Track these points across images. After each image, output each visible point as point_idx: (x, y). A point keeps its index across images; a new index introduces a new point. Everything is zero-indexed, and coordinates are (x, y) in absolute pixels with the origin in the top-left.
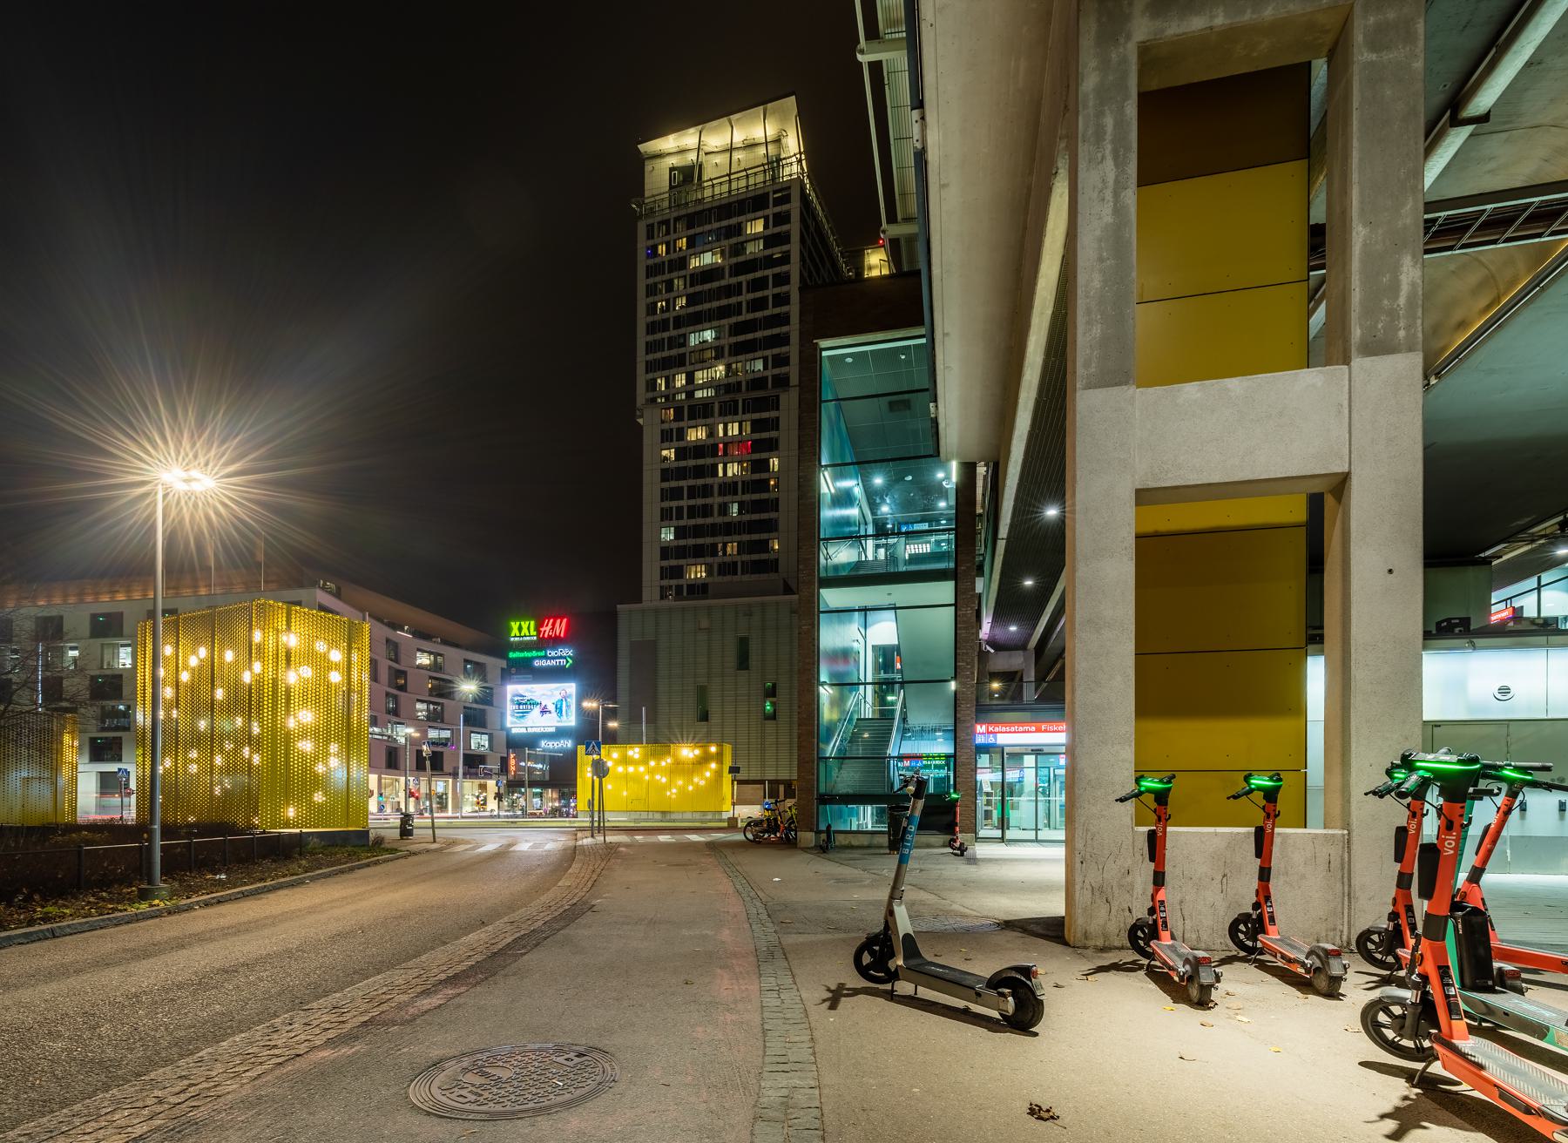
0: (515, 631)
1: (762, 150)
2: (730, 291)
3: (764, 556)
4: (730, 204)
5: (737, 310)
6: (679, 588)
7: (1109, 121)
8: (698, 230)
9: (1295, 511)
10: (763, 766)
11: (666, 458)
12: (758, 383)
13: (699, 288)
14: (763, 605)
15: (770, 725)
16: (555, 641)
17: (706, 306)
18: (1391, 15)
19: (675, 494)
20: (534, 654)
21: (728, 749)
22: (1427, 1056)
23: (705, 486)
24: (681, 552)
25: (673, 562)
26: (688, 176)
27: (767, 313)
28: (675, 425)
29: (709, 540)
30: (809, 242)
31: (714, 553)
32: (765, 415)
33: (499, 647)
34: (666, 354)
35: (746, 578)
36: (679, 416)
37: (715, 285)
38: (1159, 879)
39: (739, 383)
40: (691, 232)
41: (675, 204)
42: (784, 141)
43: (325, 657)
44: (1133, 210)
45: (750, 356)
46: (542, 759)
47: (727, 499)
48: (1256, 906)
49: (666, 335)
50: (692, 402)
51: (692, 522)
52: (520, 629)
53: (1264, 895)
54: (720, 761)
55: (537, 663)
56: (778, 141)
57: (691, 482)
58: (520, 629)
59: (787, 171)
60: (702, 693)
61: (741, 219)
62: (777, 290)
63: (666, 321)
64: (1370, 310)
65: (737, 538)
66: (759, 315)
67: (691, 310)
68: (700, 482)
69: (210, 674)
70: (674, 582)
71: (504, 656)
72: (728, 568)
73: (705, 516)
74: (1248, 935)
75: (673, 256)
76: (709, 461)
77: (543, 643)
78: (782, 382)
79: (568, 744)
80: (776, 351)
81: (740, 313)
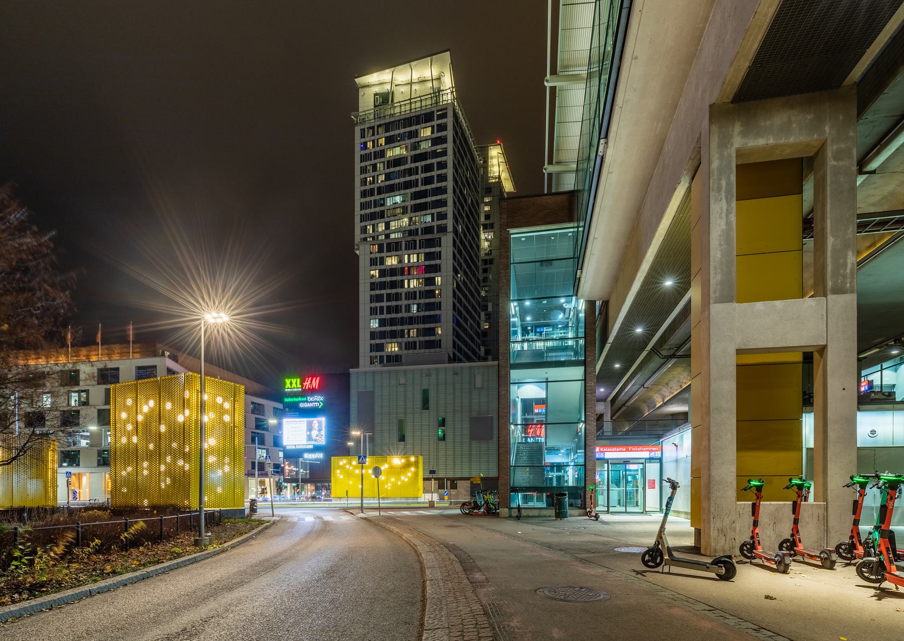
0: (288, 385)
1: (430, 84)
2: (410, 172)
3: (432, 338)
4: (411, 118)
5: (415, 183)
6: (381, 357)
7: (724, 183)
8: (392, 133)
9: (798, 357)
10: (470, 469)
11: (373, 276)
12: (428, 230)
13: (392, 170)
14: (437, 369)
15: (442, 443)
16: (312, 391)
17: (397, 181)
18: (843, 146)
19: (379, 298)
20: (300, 399)
21: (421, 458)
22: (883, 579)
23: (397, 294)
24: (383, 335)
25: (378, 341)
26: (385, 99)
27: (433, 186)
28: (378, 255)
29: (399, 328)
30: (458, 142)
31: (403, 336)
32: (433, 250)
33: (277, 395)
34: (373, 210)
35: (422, 351)
36: (381, 250)
37: (402, 168)
38: (755, 524)
39: (417, 230)
40: (388, 134)
41: (377, 117)
42: (442, 79)
43: (221, 406)
44: (734, 223)
45: (423, 212)
46: (304, 466)
47: (411, 302)
48: (792, 535)
49: (372, 198)
50: (389, 241)
51: (389, 316)
52: (291, 383)
53: (795, 530)
54: (417, 466)
55: (301, 405)
56: (439, 79)
57: (389, 291)
58: (291, 383)
59: (445, 98)
60: (401, 424)
61: (417, 127)
62: (439, 172)
63: (372, 190)
64: (835, 274)
65: (416, 326)
66: (429, 187)
67: (388, 183)
68: (394, 291)
69: (159, 416)
70: (378, 354)
71: (280, 401)
72: (411, 346)
73: (397, 312)
74: (790, 545)
75: (377, 149)
76: (399, 278)
77: (305, 392)
78: (442, 229)
79: (320, 456)
80: (439, 210)
81: (417, 186)
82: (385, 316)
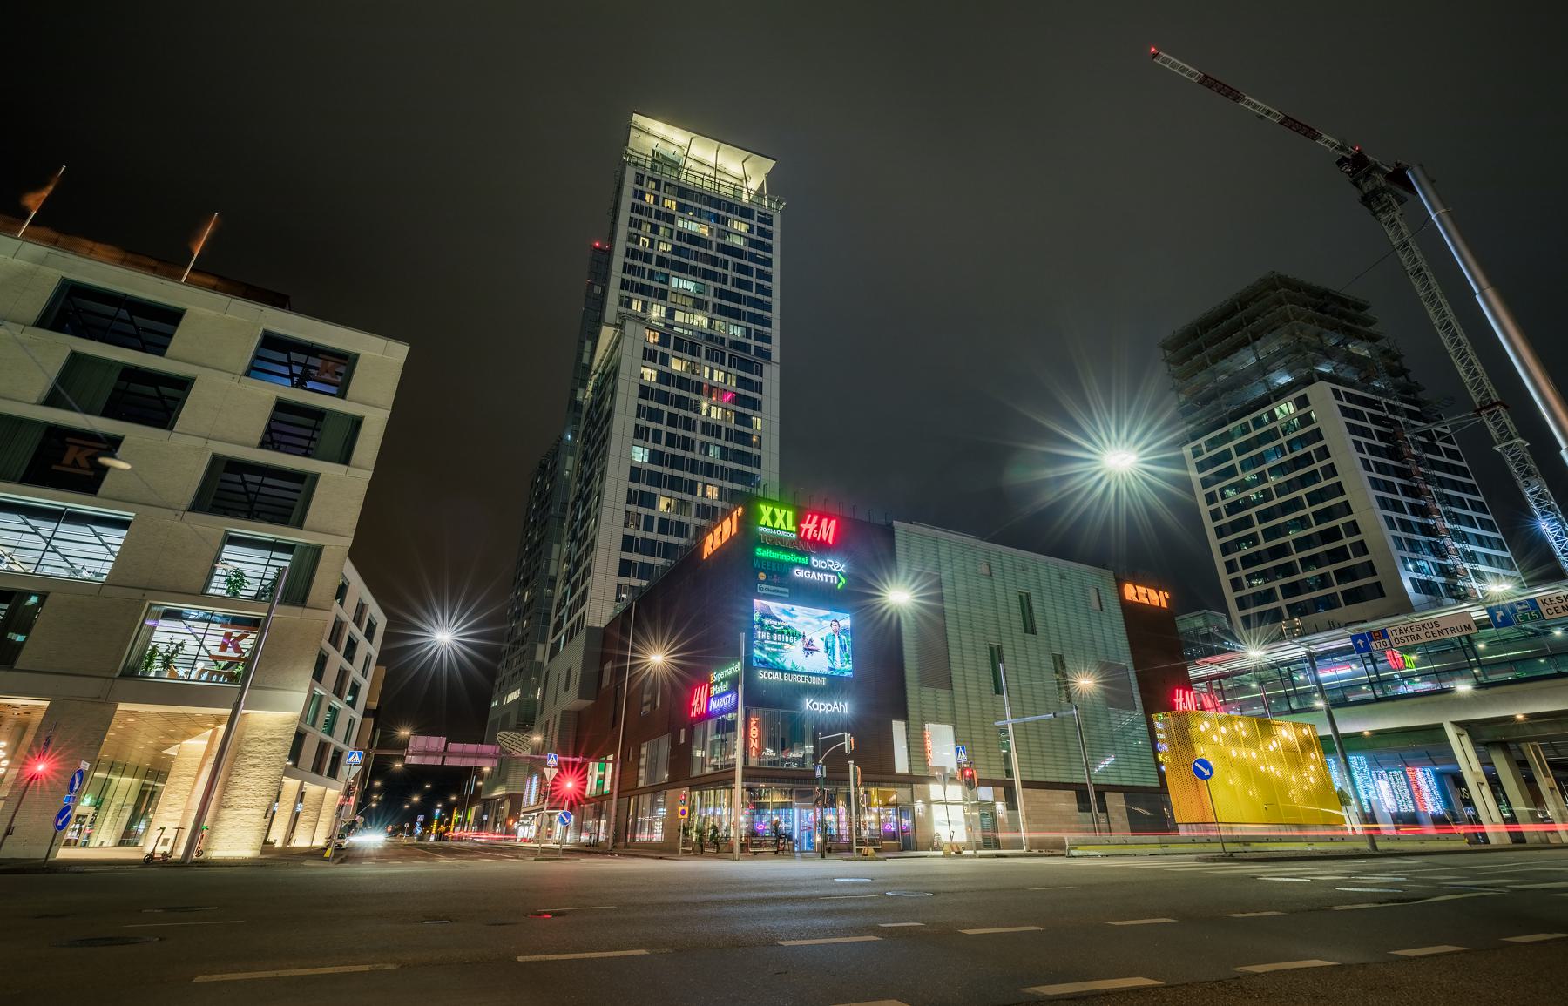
0: (765, 519)
16: (821, 547)
20: (793, 558)
29: (688, 476)
47: (711, 439)
52: (773, 517)
55: (798, 573)
57: (674, 410)
58: (773, 517)
70: (644, 511)
73: (685, 448)
77: (809, 546)
82: (660, 447)
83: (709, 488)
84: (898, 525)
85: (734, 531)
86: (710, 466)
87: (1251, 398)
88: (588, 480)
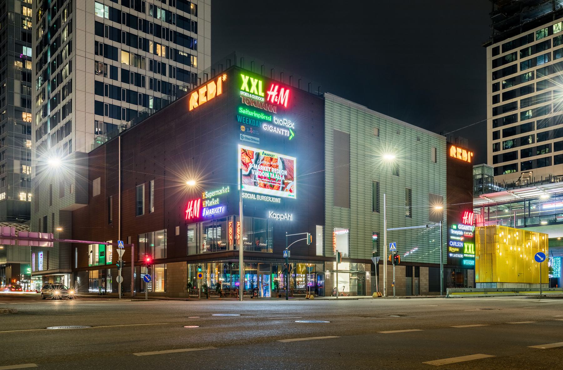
0: (244, 86)
16: (280, 109)
20: (261, 116)
29: (141, 34)
52: (249, 84)
55: (265, 127)
58: (249, 84)
70: (109, 62)
77: (270, 107)
83: (159, 47)
84: (326, 95)
85: (220, 92)
86: (158, 27)
87: (541, 15)
88: (53, 30)
